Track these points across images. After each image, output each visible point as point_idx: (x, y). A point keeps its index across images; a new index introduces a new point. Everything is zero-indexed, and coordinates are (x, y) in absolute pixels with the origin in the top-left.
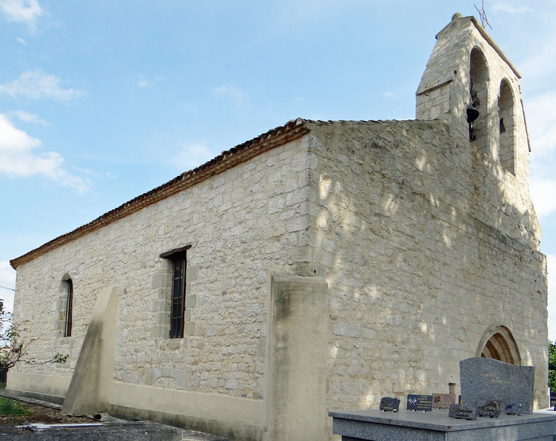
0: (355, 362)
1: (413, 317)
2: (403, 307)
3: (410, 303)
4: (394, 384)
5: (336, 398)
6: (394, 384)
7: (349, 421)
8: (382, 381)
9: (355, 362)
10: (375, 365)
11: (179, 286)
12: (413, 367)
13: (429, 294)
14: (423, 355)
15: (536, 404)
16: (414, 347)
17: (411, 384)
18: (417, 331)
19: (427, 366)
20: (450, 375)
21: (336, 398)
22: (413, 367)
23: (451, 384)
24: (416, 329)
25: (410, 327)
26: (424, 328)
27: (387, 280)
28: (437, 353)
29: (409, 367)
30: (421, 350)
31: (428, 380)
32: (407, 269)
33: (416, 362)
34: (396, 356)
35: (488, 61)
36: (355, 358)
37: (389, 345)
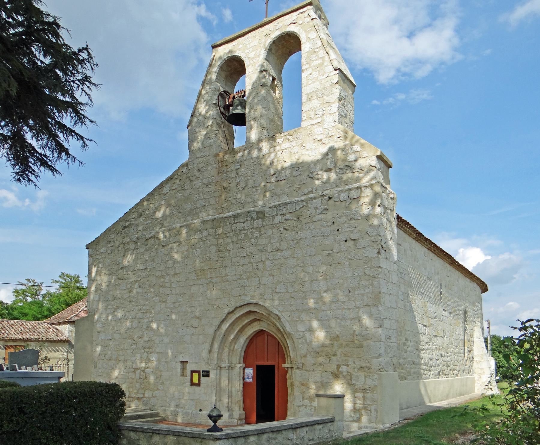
0: (109, 352)
1: (146, 320)
2: (139, 315)
3: (144, 312)
4: (133, 363)
5: (100, 371)
6: (133, 363)
7: (279, 433)
8: (125, 361)
9: (109, 352)
10: (120, 353)
11: (266, 356)
12: (147, 352)
13: (160, 301)
14: (154, 343)
15: (252, 373)
16: (147, 339)
17: (146, 363)
18: (149, 329)
19: (157, 351)
20: (181, 355)
21: (100, 371)
22: (147, 352)
23: (182, 362)
24: (149, 328)
25: (144, 327)
26: (154, 326)
27: (128, 303)
28: (167, 340)
29: (144, 352)
30: (153, 340)
31: (159, 360)
32: (141, 291)
33: (149, 348)
34: (134, 346)
35: (314, 13)
36: (110, 350)
37: (129, 341)
